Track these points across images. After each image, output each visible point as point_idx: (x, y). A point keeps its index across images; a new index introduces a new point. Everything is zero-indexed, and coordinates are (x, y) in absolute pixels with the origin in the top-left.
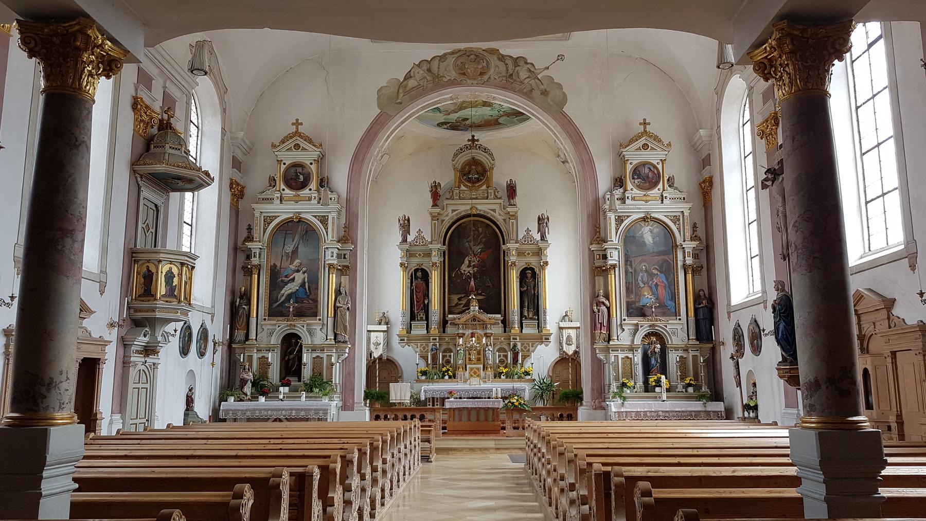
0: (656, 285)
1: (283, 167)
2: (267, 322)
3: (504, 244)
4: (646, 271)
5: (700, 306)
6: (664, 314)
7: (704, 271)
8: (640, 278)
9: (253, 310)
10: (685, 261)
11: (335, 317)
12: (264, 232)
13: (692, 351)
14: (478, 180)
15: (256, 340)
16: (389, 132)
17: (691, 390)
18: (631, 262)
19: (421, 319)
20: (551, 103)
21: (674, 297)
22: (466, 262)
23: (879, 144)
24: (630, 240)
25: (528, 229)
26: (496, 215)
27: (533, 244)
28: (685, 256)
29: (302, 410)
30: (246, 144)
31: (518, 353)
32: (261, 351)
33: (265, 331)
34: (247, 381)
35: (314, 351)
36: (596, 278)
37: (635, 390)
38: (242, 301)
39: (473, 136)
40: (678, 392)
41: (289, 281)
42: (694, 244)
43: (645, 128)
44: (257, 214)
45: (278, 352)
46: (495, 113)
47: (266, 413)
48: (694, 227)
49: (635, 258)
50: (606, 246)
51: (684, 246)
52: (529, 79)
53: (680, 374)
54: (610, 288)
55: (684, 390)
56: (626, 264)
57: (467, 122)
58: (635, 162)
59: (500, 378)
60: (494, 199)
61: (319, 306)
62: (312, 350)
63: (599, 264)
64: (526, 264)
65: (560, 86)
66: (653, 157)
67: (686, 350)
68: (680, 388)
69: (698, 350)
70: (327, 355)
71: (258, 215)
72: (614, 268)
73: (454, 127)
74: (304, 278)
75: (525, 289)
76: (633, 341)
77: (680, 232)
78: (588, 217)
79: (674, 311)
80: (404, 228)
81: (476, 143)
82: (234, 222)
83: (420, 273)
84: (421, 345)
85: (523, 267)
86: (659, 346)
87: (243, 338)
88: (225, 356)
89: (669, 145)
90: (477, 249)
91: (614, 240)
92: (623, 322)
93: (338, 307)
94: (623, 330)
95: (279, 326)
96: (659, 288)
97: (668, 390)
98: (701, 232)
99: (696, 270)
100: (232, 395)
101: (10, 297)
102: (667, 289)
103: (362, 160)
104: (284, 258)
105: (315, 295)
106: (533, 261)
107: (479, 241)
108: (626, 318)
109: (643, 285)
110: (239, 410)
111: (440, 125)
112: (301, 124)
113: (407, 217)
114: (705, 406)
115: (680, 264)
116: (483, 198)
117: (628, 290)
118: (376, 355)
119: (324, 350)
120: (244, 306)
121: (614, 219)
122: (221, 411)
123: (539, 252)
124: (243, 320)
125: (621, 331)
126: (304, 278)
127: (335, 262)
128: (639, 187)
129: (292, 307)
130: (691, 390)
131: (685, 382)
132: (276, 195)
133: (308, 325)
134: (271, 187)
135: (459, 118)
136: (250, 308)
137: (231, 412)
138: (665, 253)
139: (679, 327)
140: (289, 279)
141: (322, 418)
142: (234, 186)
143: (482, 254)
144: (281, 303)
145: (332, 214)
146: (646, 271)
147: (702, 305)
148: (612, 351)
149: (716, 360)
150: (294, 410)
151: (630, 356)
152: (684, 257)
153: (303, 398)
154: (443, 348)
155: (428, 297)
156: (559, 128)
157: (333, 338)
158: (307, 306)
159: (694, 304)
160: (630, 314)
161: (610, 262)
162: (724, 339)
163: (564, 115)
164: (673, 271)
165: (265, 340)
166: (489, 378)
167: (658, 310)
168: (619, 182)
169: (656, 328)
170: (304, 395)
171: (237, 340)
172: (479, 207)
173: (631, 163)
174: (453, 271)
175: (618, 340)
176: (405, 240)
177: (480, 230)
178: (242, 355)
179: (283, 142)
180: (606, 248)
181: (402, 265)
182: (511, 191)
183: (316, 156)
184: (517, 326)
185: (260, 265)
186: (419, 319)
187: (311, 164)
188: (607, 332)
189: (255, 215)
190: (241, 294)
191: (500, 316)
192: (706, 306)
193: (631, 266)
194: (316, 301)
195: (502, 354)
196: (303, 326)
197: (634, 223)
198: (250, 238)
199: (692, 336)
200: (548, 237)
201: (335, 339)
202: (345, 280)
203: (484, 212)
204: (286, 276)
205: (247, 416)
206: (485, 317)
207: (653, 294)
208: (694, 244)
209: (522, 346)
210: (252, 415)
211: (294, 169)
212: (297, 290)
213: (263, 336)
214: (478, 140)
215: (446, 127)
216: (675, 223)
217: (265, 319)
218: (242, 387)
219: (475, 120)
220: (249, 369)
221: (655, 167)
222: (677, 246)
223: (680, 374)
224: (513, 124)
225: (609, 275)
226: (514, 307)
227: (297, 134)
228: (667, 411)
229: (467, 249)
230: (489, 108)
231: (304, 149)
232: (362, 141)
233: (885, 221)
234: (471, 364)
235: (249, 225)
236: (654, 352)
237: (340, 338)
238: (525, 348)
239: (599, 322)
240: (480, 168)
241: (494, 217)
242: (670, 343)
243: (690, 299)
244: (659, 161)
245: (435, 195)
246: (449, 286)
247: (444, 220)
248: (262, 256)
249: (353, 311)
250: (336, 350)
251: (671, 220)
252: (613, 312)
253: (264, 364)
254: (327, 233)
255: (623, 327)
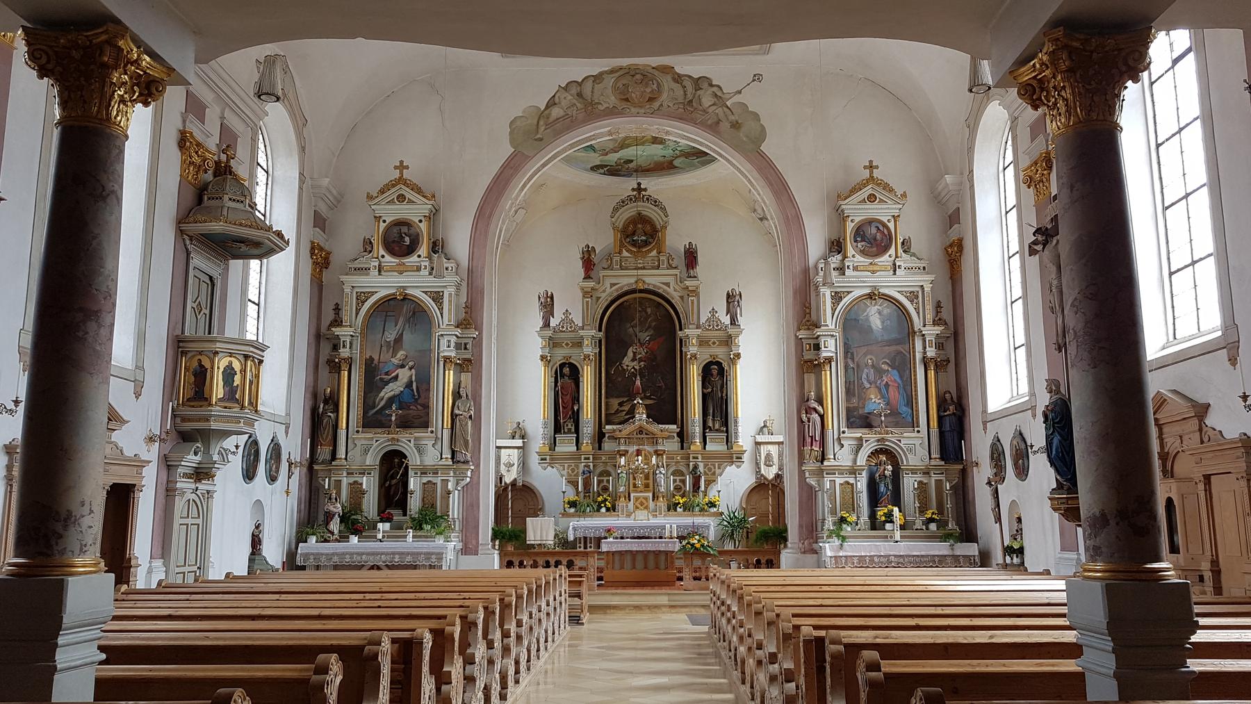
0: (887, 385)
1: (382, 226)
2: (361, 435)
3: (681, 330)
4: (873, 366)
5: (946, 414)
6: (897, 425)
7: (952, 366)
8: (864, 376)
9: (342, 418)
10: (925, 353)
11: (452, 428)
12: (357, 314)
13: (934, 474)
14: (646, 243)
15: (346, 459)
16: (526, 178)
17: (933, 526)
18: (852, 354)
19: (569, 431)
20: (744, 139)
21: (911, 401)
22: (630, 354)
23: (1187, 195)
24: (851, 324)
25: (713, 309)
26: (671, 290)
27: (719, 330)
28: (925, 346)
29: (408, 554)
30: (333, 195)
31: (700, 476)
32: (352, 474)
33: (358, 447)
34: (334, 515)
35: (424, 474)
36: (806, 376)
37: (858, 527)
38: (327, 407)
39: (639, 184)
40: (916, 530)
41: (391, 379)
42: (938, 330)
43: (871, 173)
44: (347, 290)
45: (375, 475)
46: (668, 153)
47: (359, 558)
48: (938, 306)
49: (858, 349)
50: (818, 332)
51: (923, 333)
52: (715, 107)
53: (918, 505)
54: (824, 389)
55: (924, 527)
56: (846, 357)
57: (631, 165)
58: (857, 219)
59: (676, 510)
60: (668, 269)
61: (431, 414)
62: (422, 473)
63: (809, 357)
64: (711, 356)
65: (756, 117)
66: (882, 212)
67: (926, 473)
68: (919, 524)
69: (943, 474)
70: (442, 480)
71: (349, 290)
72: (830, 362)
73: (613, 171)
74: (411, 376)
75: (710, 390)
76: (855, 461)
77: (918, 313)
78: (795, 293)
79: (910, 420)
80: (546, 308)
81: (644, 193)
82: (316, 300)
83: (568, 369)
84: (569, 466)
85: (707, 361)
86: (890, 467)
87: (328, 457)
88: (304, 481)
89: (904, 195)
90: (645, 336)
91: (830, 325)
92: (842, 435)
93: (457, 416)
94: (842, 446)
95: (377, 441)
96: (891, 389)
97: (903, 527)
98: (947, 314)
99: (940, 365)
100: (313, 534)
101: (13, 401)
102: (902, 390)
103: (490, 217)
104: (384, 349)
105: (425, 398)
106: (720, 353)
107: (647, 325)
108: (846, 429)
109: (869, 386)
110: (322, 554)
111: (594, 169)
112: (407, 167)
113: (549, 294)
114: (952, 549)
115: (918, 356)
116: (653, 268)
117: (849, 392)
118: (508, 479)
119: (437, 473)
120: (329, 414)
121: (830, 296)
122: (298, 556)
123: (728, 341)
124: (328, 432)
125: (839, 448)
126: (411, 376)
127: (453, 354)
128: (863, 253)
129: (394, 414)
130: (933, 526)
131: (926, 516)
132: (373, 264)
133: (416, 439)
134: (366, 253)
135: (619, 159)
136: (337, 416)
137: (312, 557)
138: (898, 342)
139: (918, 442)
140: (390, 377)
141: (434, 565)
142: (316, 251)
143: (651, 343)
144: (380, 409)
145: (449, 289)
146: (873, 366)
147: (948, 413)
148: (827, 474)
149: (968, 487)
150: (397, 554)
151: (852, 481)
152: (925, 348)
153: (410, 538)
154: (598, 471)
155: (578, 401)
156: (755, 173)
157: (449, 456)
158: (415, 413)
159: (938, 411)
160: (851, 425)
161: (825, 354)
162: (978, 458)
163: (762, 155)
164: (909, 366)
165: (358, 459)
166: (660, 511)
167: (889, 419)
168: (836, 246)
169: (887, 443)
170: (411, 534)
171: (321, 459)
172: (647, 280)
173: (852, 221)
174: (612, 367)
175: (835, 459)
176: (547, 325)
177: (649, 310)
178: (327, 480)
179: (382, 192)
180: (819, 336)
181: (543, 358)
182: (691, 258)
183: (428, 211)
184: (698, 441)
185: (351, 358)
186: (566, 431)
187: (420, 221)
188: (820, 448)
189: (345, 290)
190: (325, 397)
191: (675, 426)
192: (954, 414)
193: (853, 359)
194: (426, 407)
195: (678, 478)
196: (410, 441)
197: (857, 301)
198: (337, 322)
199: (935, 455)
200: (741, 320)
201: (453, 458)
202: (466, 378)
203: (654, 286)
204: (387, 374)
205: (334, 562)
206: (655, 428)
207: (883, 397)
208: (938, 330)
209: (705, 468)
210: (341, 560)
211: (398, 228)
212: (402, 392)
213: (355, 454)
214: (645, 190)
215: (602, 171)
216: (912, 302)
217: (358, 432)
218: (327, 523)
219: (641, 162)
220: (336, 499)
221: (885, 225)
222: (915, 333)
223: (918, 505)
224: (693, 167)
225: (823, 372)
226: (695, 415)
227: (401, 180)
228: (901, 556)
229: (631, 336)
230: (661, 146)
231: (410, 202)
232: (490, 190)
233: (1196, 299)
234: (637, 492)
235: (337, 303)
236: (884, 475)
237: (459, 457)
238: (710, 470)
239: (809, 436)
240: (648, 228)
241: (668, 294)
242: (905, 463)
243: (932, 404)
244: (890, 218)
245: (588, 264)
246: (606, 386)
247: (600, 298)
248: (354, 347)
249: (477, 420)
250: (455, 473)
251: (907, 297)
252: (828, 421)
253: (357, 492)
254: (442, 314)
255: (842, 442)
